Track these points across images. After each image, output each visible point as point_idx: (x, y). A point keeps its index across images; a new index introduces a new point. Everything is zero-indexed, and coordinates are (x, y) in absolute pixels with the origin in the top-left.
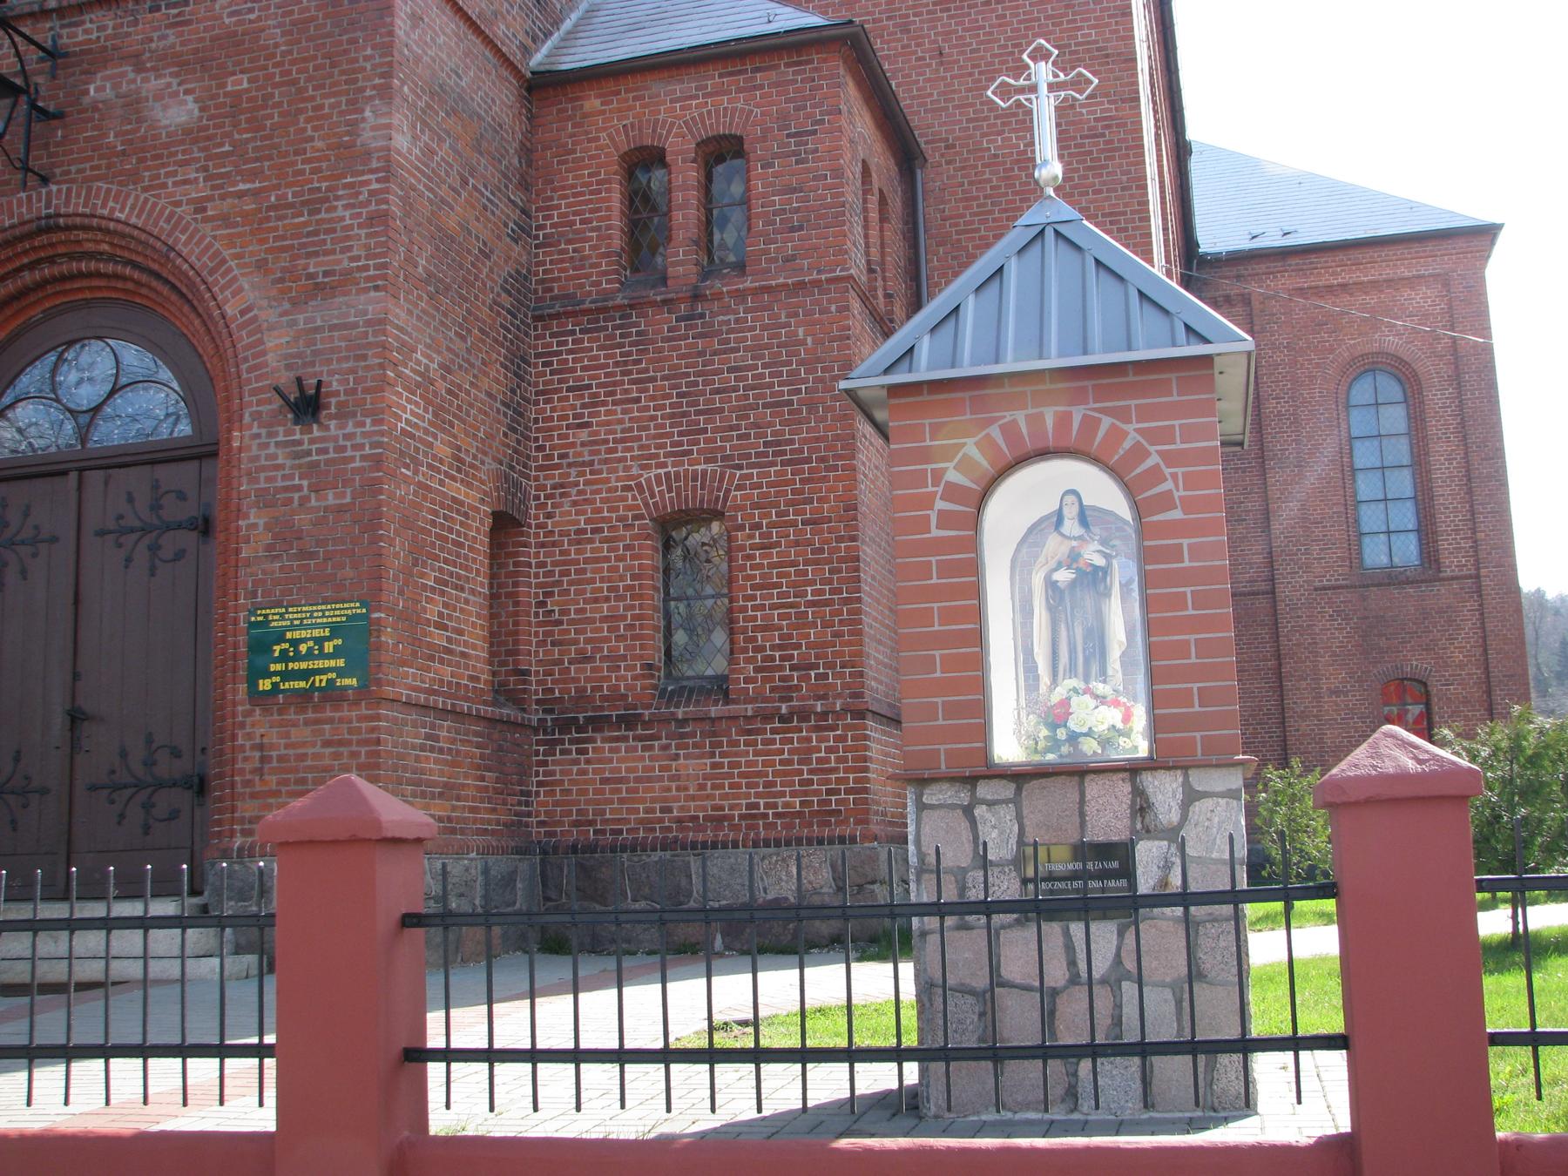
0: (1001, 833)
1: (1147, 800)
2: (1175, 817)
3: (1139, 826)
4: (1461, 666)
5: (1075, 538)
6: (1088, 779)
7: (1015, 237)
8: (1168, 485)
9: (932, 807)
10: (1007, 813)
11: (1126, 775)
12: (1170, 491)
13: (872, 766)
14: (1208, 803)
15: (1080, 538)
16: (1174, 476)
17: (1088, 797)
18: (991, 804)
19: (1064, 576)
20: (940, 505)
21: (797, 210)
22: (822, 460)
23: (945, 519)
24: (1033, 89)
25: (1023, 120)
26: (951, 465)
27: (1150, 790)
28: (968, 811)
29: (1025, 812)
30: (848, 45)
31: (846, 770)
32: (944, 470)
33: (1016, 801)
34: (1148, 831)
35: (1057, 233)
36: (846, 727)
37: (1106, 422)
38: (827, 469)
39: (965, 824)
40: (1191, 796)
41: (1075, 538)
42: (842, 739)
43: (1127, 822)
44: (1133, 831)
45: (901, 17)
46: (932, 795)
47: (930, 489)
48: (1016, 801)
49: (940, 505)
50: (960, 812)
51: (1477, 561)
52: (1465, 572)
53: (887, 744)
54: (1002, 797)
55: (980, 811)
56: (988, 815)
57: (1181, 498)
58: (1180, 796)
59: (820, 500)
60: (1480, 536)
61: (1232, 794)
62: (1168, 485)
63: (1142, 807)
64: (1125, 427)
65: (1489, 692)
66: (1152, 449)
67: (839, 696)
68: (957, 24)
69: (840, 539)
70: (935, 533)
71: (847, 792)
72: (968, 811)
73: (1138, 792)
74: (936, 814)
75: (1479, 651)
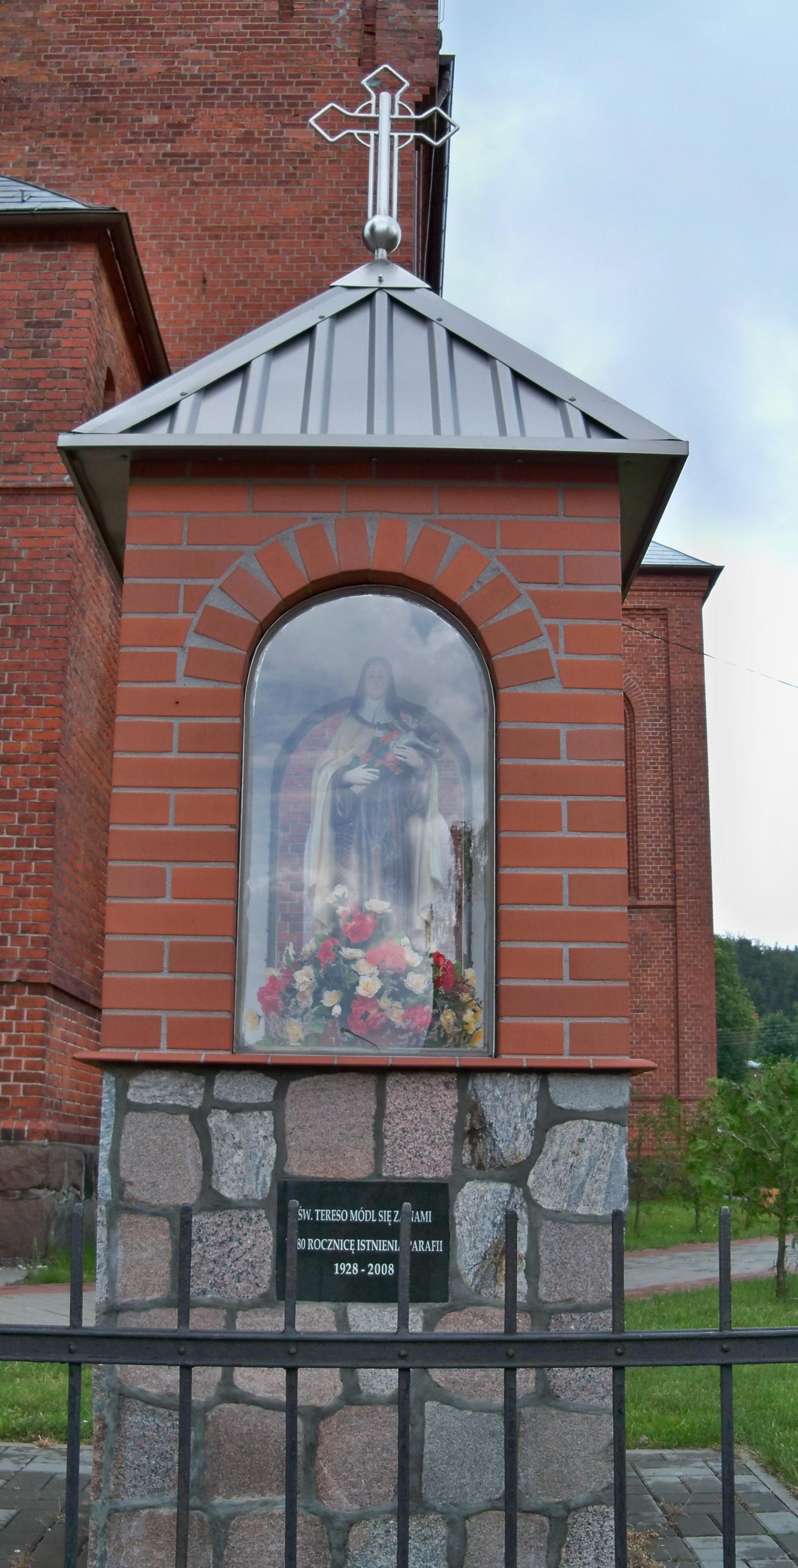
0: (249, 1156)
1: (482, 1119)
2: (523, 1147)
3: (466, 1158)
4: (653, 994)
5: (379, 726)
6: (391, 1080)
7: (335, 299)
8: (543, 643)
9: (141, 1108)
10: (261, 1126)
11: (453, 1078)
12: (546, 651)
13: (50, 1051)
14: (575, 1128)
15: (388, 727)
16: (553, 631)
17: (390, 1108)
18: (235, 1109)
19: (361, 775)
20: (195, 641)
21: (28, 408)
22: (24, 690)
23: (200, 665)
24: (374, 123)
25: (356, 161)
26: (217, 583)
27: (487, 1104)
28: (198, 1118)
29: (289, 1125)
30: (106, 237)
31: (19, 1053)
32: (207, 589)
33: (276, 1106)
34: (480, 1167)
35: (393, 301)
36: (23, 1003)
37: (457, 541)
38: (29, 702)
39: (192, 1139)
40: (550, 1117)
41: (379, 726)
42: (17, 1015)
43: (448, 1150)
44: (457, 1165)
45: (166, 237)
46: (144, 1090)
47: (181, 615)
48: (276, 1106)
49: (195, 641)
50: (185, 1118)
51: (675, 890)
52: (662, 902)
53: (68, 1026)
54: (254, 1100)
55: (217, 1120)
56: (229, 1127)
57: (559, 662)
58: (532, 1115)
59: (17, 736)
60: (679, 867)
61: (608, 1116)
62: (543, 643)
63: (473, 1129)
64: (485, 552)
65: (677, 1021)
66: (522, 588)
67: (17, 964)
68: (225, 253)
69: (35, 783)
70: (182, 683)
71: (17, 1078)
72: (198, 1118)
73: (469, 1107)
74: (145, 1119)
75: (670, 980)
